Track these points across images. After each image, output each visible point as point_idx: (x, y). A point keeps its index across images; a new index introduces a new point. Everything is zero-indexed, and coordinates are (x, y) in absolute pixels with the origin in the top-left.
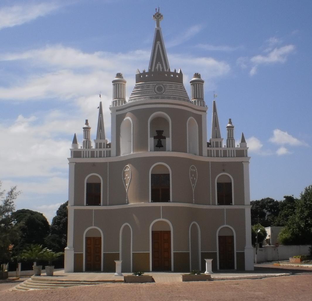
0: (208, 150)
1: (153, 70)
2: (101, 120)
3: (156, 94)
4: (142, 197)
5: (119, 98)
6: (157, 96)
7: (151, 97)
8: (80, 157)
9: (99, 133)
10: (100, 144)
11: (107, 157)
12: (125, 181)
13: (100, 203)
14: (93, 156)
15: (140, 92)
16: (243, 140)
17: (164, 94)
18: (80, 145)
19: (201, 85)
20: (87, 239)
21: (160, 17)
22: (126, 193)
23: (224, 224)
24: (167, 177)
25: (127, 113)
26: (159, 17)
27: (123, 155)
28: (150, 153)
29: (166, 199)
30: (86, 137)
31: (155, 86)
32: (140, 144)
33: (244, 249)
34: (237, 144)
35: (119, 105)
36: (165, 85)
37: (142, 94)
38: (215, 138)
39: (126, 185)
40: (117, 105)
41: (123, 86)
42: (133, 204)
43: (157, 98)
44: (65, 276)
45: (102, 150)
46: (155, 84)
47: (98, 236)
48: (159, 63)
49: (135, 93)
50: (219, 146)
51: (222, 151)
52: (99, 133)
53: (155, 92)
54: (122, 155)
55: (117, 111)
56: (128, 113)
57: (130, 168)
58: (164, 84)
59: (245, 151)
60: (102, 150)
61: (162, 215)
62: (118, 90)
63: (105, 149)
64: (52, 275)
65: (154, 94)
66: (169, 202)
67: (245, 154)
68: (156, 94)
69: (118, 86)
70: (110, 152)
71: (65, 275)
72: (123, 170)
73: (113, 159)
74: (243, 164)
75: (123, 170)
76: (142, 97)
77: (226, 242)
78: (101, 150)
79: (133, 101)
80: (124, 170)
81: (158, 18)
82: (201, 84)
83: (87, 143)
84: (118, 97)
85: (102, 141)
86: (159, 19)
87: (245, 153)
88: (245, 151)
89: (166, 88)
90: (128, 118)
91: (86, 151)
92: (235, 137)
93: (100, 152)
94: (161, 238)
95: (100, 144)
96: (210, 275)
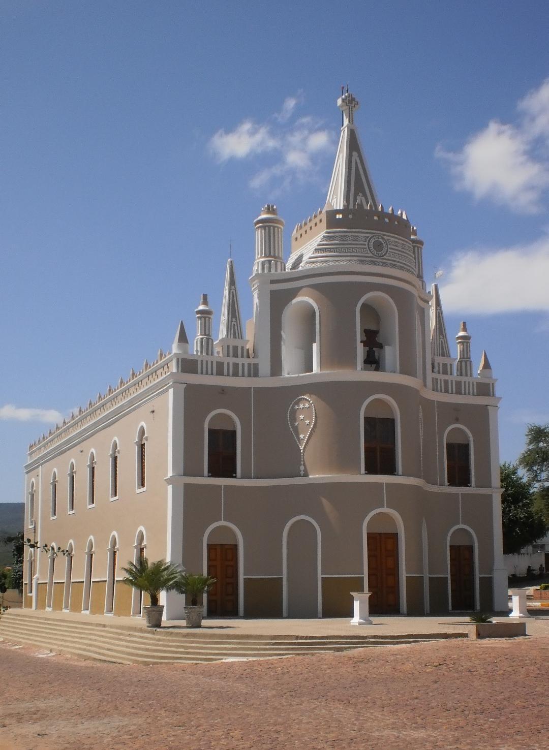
0: (433, 378)
1: (351, 207)
2: (233, 299)
3: (371, 255)
4: (343, 462)
5: (274, 257)
6: (373, 259)
7: (361, 261)
8: (195, 372)
9: (231, 325)
10: (235, 348)
11: (249, 376)
12: (296, 430)
13: (234, 471)
14: (220, 373)
15: (336, 248)
16: (487, 366)
17: (385, 257)
18: (195, 348)
19: (418, 250)
20: (211, 547)
21: (355, 104)
22: (301, 453)
23: (459, 524)
24: (390, 423)
25: (301, 288)
26: (353, 105)
27: (288, 374)
28: (359, 374)
29: (390, 469)
30: (205, 331)
31: (370, 240)
32: (337, 354)
33: (491, 570)
34: (478, 367)
35: (276, 270)
36: (388, 240)
37: (354, 252)
38: (441, 355)
39: (298, 438)
40: (273, 271)
41: (278, 232)
42: (316, 476)
43: (374, 263)
44: (231, 627)
45: (240, 361)
46: (370, 236)
47: (230, 542)
48: (360, 194)
49: (326, 249)
50: (449, 372)
51: (475, 384)
52: (231, 325)
53: (370, 250)
54: (285, 374)
55: (272, 282)
56: (304, 289)
57: (312, 403)
58: (386, 238)
59: (491, 384)
60: (240, 361)
61: (388, 501)
62: (272, 241)
63: (246, 361)
64: (199, 626)
65: (367, 255)
66: (395, 475)
67: (491, 393)
68: (371, 255)
69: (272, 233)
70: (256, 366)
71: (231, 626)
72: (291, 405)
73: (265, 381)
74: (488, 410)
75: (291, 405)
76: (344, 259)
77: (462, 556)
78: (235, 360)
79: (318, 265)
80: (293, 406)
81: (351, 105)
82: (418, 247)
83: (207, 344)
84: (272, 254)
85: (238, 343)
86: (353, 108)
87: (491, 390)
88: (491, 384)
89: (389, 246)
90: (304, 299)
91: (207, 361)
92: (473, 358)
93: (236, 365)
94: (383, 546)
95: (235, 348)
96: (524, 624)
